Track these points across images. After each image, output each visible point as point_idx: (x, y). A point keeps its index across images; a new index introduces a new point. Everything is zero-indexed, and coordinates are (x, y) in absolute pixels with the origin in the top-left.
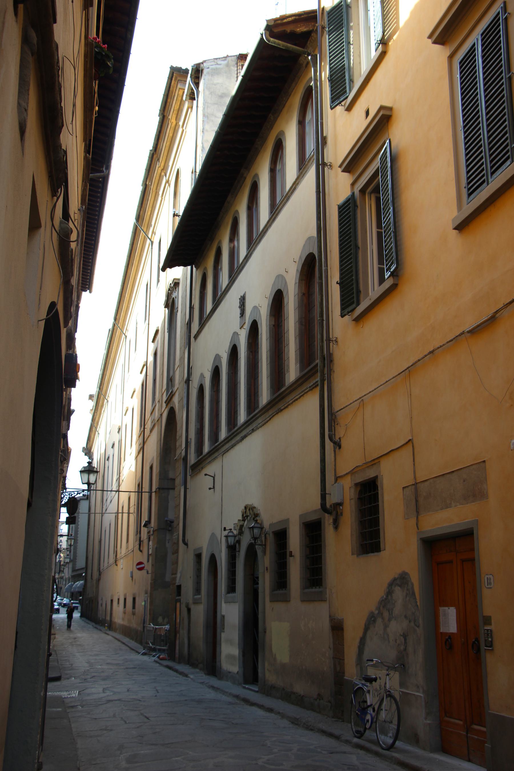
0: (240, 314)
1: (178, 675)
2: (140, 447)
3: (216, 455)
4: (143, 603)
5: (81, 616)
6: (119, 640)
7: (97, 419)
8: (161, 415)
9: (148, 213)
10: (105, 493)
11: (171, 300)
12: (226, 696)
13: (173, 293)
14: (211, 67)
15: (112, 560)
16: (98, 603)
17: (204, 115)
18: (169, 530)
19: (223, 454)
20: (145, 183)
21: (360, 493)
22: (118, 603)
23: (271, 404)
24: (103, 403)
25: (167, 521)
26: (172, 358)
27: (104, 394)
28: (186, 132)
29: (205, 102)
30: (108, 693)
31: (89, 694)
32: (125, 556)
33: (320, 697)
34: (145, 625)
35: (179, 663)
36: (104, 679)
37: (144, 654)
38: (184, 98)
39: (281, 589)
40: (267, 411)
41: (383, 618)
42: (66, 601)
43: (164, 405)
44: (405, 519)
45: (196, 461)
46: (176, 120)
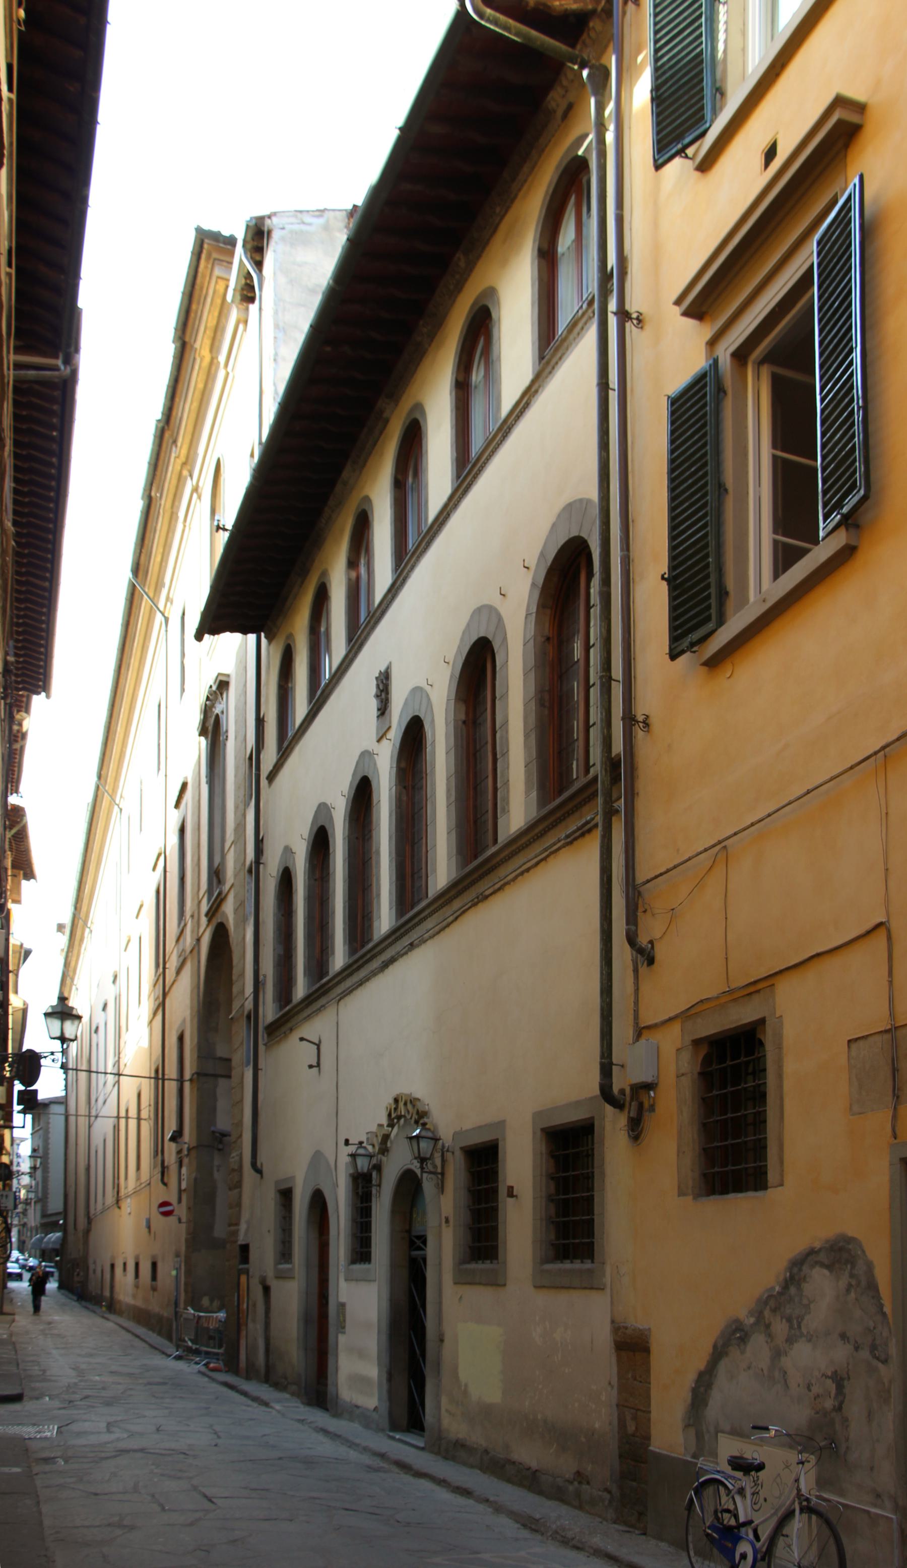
0: (379, 710)
1: (250, 1402)
2: (157, 1003)
3: (322, 1001)
4: (174, 1273)
5: (60, 1287)
6: (128, 1331)
7: (73, 964)
8: (198, 940)
9: (156, 558)
10: (94, 1075)
11: (212, 720)
12: (355, 1450)
13: (217, 705)
14: (288, 227)
15: (110, 1199)
16: (88, 1268)
17: (277, 326)
18: (219, 1150)
19: (339, 1000)
20: (147, 493)
21: (707, 1061)
22: (125, 1269)
23: (456, 889)
24: (83, 934)
25: (213, 1132)
26: (217, 832)
27: (83, 918)
28: (234, 377)
29: (278, 300)
30: (118, 1434)
31: (79, 1434)
32: (134, 1192)
33: (580, 1477)
34: (178, 1309)
35: (248, 1378)
36: (108, 1404)
37: (178, 1358)
38: (229, 298)
39: (481, 1262)
40: (450, 901)
41: (770, 1336)
42: (32, 1262)
43: (204, 920)
44: (852, 1115)
45: (278, 1016)
46: (211, 351)
